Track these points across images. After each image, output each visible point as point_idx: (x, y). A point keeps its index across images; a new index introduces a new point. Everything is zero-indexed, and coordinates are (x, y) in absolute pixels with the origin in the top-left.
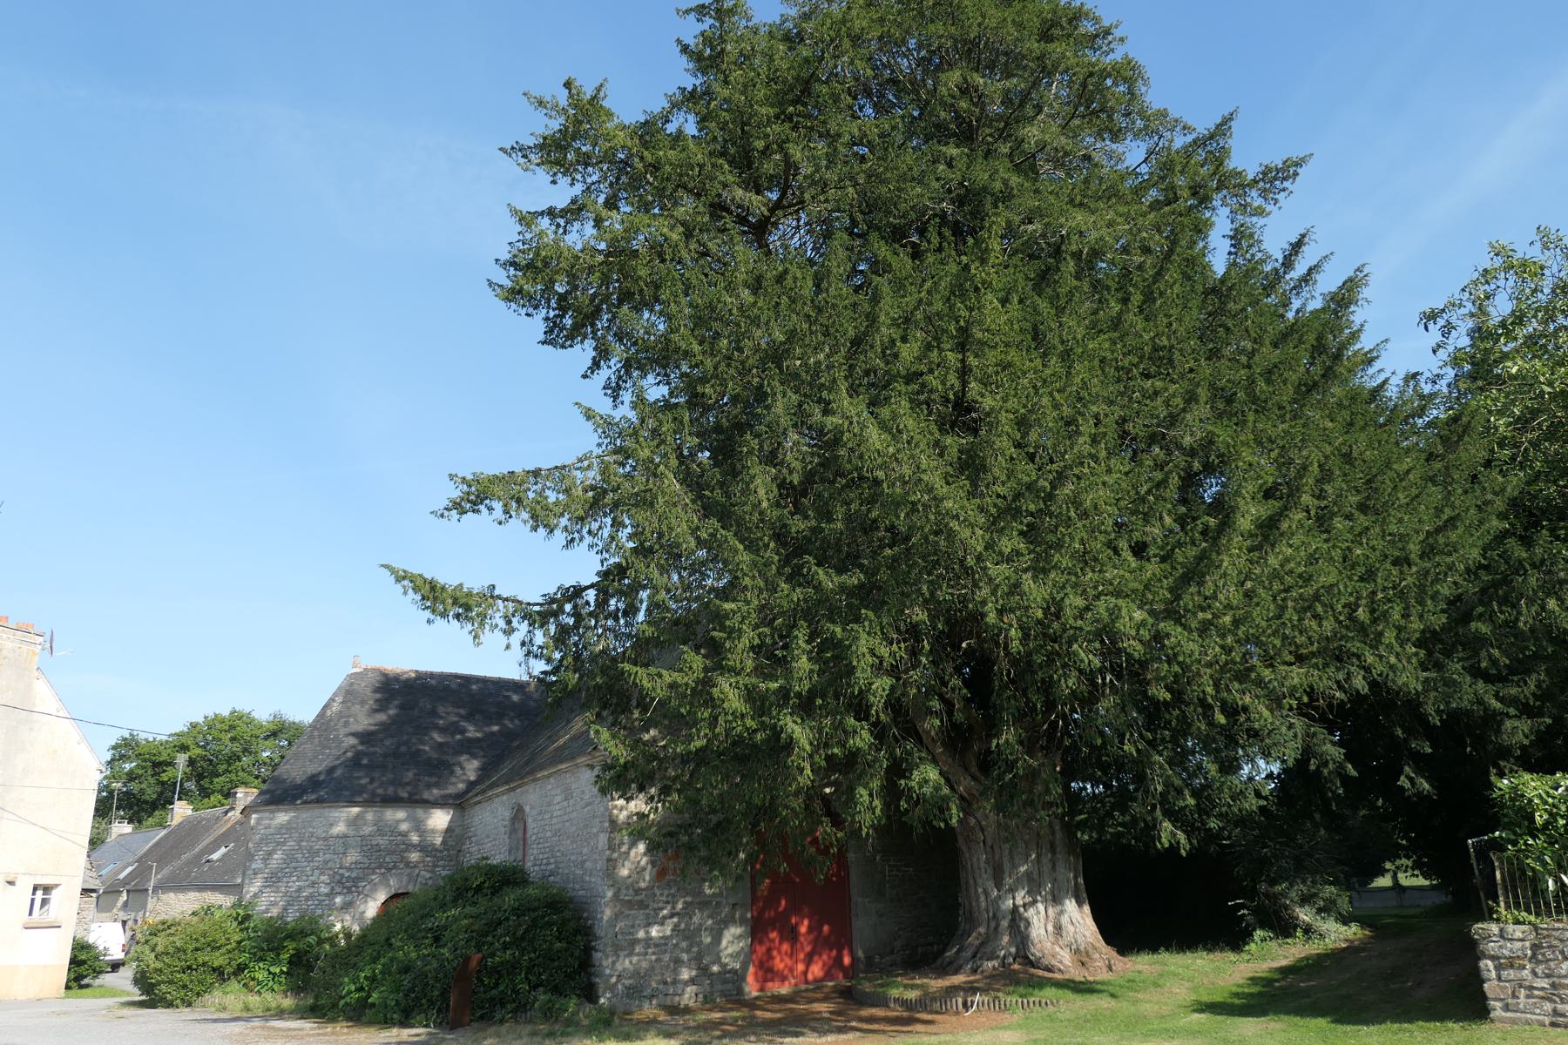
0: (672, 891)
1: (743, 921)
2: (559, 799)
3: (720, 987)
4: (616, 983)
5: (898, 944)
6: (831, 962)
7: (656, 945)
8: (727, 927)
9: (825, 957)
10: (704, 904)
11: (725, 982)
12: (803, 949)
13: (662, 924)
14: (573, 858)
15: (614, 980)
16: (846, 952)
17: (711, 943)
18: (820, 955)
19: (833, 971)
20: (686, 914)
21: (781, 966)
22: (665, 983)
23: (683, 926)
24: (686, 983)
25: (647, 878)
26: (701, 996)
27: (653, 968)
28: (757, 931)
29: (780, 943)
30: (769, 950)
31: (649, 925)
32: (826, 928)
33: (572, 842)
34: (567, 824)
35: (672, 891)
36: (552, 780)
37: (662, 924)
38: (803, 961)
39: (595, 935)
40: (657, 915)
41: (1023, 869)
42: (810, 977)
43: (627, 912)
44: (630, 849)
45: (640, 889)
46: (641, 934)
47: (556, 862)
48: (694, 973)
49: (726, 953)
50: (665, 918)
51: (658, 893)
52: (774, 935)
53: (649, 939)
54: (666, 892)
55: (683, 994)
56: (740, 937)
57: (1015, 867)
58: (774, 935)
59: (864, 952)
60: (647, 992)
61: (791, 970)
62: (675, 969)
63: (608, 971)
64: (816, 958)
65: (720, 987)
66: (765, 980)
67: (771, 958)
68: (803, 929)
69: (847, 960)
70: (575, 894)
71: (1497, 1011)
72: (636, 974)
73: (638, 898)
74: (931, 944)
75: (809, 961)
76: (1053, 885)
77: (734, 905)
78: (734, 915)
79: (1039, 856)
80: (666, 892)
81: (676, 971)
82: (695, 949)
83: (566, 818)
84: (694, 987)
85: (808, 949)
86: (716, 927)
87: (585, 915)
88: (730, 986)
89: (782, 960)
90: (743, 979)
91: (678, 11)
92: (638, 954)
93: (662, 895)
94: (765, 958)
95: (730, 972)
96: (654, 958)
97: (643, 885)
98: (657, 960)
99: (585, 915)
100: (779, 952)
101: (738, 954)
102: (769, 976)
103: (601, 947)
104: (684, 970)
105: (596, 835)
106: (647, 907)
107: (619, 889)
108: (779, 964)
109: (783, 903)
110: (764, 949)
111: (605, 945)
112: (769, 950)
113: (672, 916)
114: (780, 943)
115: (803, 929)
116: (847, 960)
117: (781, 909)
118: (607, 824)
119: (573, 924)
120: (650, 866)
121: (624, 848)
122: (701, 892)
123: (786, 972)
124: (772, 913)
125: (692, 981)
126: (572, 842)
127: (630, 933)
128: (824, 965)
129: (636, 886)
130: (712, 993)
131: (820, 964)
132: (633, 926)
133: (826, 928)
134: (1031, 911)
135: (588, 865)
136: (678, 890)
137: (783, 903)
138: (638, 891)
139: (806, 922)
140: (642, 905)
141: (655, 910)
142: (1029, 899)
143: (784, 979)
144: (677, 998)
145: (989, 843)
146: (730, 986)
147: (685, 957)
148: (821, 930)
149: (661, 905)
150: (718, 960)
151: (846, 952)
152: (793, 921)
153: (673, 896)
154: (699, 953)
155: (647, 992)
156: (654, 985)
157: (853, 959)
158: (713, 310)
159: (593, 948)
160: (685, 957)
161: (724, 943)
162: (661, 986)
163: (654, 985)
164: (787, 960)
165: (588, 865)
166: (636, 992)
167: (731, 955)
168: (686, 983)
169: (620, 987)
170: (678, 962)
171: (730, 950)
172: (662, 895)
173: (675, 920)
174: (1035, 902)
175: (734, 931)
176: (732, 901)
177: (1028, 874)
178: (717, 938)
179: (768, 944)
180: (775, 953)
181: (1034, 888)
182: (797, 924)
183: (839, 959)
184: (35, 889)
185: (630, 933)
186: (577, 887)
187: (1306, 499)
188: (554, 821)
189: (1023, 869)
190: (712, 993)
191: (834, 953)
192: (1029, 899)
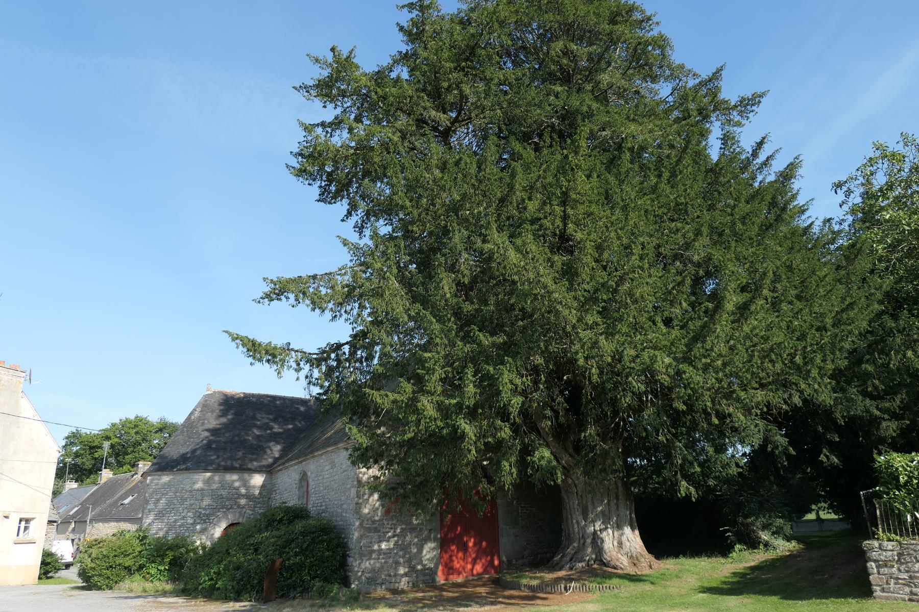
0: (394, 522)
1: (435, 540)
2: (327, 468)
3: (422, 578)
4: (361, 576)
5: (526, 553)
6: (487, 563)
7: (385, 554)
8: (426, 543)
9: (483, 560)
10: (413, 529)
11: (425, 575)
12: (470, 556)
13: (388, 541)
14: (336, 502)
15: (360, 574)
16: (496, 558)
17: (417, 552)
18: (481, 559)
19: (488, 569)
20: (402, 535)
21: (458, 566)
22: (390, 576)
23: (400, 542)
24: (402, 576)
25: (379, 514)
26: (411, 583)
27: (382, 567)
28: (444, 545)
29: (457, 552)
30: (451, 556)
31: (380, 542)
32: (484, 544)
33: (335, 493)
34: (332, 483)
35: (394, 522)
36: (323, 457)
37: (388, 541)
38: (471, 563)
39: (349, 548)
40: (385, 536)
41: (599, 509)
42: (475, 572)
43: (368, 534)
44: (369, 497)
45: (375, 521)
46: (376, 547)
47: (326, 505)
48: (407, 570)
49: (426, 558)
50: (390, 537)
51: (386, 523)
52: (453, 548)
53: (380, 550)
54: (390, 523)
55: (400, 582)
56: (433, 549)
57: (595, 508)
58: (453, 548)
59: (506, 558)
60: (379, 581)
61: (464, 568)
62: (396, 568)
63: (356, 569)
64: (478, 561)
65: (422, 578)
66: (449, 574)
67: (452, 561)
68: (471, 544)
69: (496, 562)
70: (337, 523)
71: (878, 592)
72: (373, 570)
73: (374, 526)
74: (546, 553)
75: (474, 563)
76: (617, 518)
77: (430, 530)
78: (430, 536)
79: (609, 501)
80: (390, 523)
81: (396, 569)
82: (407, 556)
83: (332, 479)
84: (407, 578)
85: (474, 556)
86: (420, 543)
87: (343, 536)
88: (428, 578)
89: (458, 562)
90: (436, 573)
91: (397, 6)
92: (374, 559)
93: (388, 524)
94: (448, 561)
95: (428, 569)
96: (383, 561)
97: (377, 518)
98: (385, 562)
99: (343, 536)
100: (457, 557)
101: (433, 558)
102: (451, 571)
103: (352, 555)
104: (401, 568)
105: (349, 489)
106: (379, 531)
107: (363, 521)
108: (457, 565)
109: (459, 529)
110: (448, 556)
111: (355, 553)
112: (451, 556)
113: (394, 536)
114: (457, 552)
115: (471, 544)
116: (496, 562)
117: (457, 532)
118: (356, 483)
119: (336, 541)
120: (381, 507)
121: (366, 497)
122: (411, 523)
123: (460, 569)
124: (453, 535)
125: (406, 575)
126: (335, 493)
127: (369, 547)
128: (483, 565)
129: (373, 519)
130: (417, 582)
131: (481, 564)
132: (371, 543)
133: (484, 544)
134: (604, 534)
135: (345, 506)
136: (398, 521)
137: (459, 529)
138: (374, 522)
139: (472, 540)
140: (376, 530)
141: (384, 533)
142: (603, 527)
143: (459, 573)
144: (397, 585)
145: (580, 494)
146: (428, 578)
147: (401, 560)
148: (481, 545)
149: (387, 530)
150: (421, 562)
151: (496, 558)
152: (465, 539)
153: (395, 525)
154: (410, 558)
155: (379, 581)
156: (383, 577)
157: (500, 562)
158: (418, 181)
159: (348, 555)
160: (401, 560)
161: (424, 552)
162: (387, 578)
163: (383, 577)
164: (461, 562)
165: (345, 506)
166: (373, 581)
167: (428, 559)
168: (402, 576)
169: (363, 578)
170: (397, 563)
171: (428, 557)
172: (388, 524)
173: (396, 539)
174: (606, 528)
175: (430, 545)
176: (429, 527)
177: (602, 512)
178: (420, 550)
179: (450, 553)
180: (454, 558)
181: (606, 520)
182: (467, 541)
183: (492, 562)
184: (21, 520)
185: (369, 547)
186: (338, 519)
187: (765, 292)
188: (325, 481)
189: (599, 509)
190: (417, 582)
191: (489, 558)
192: (603, 527)
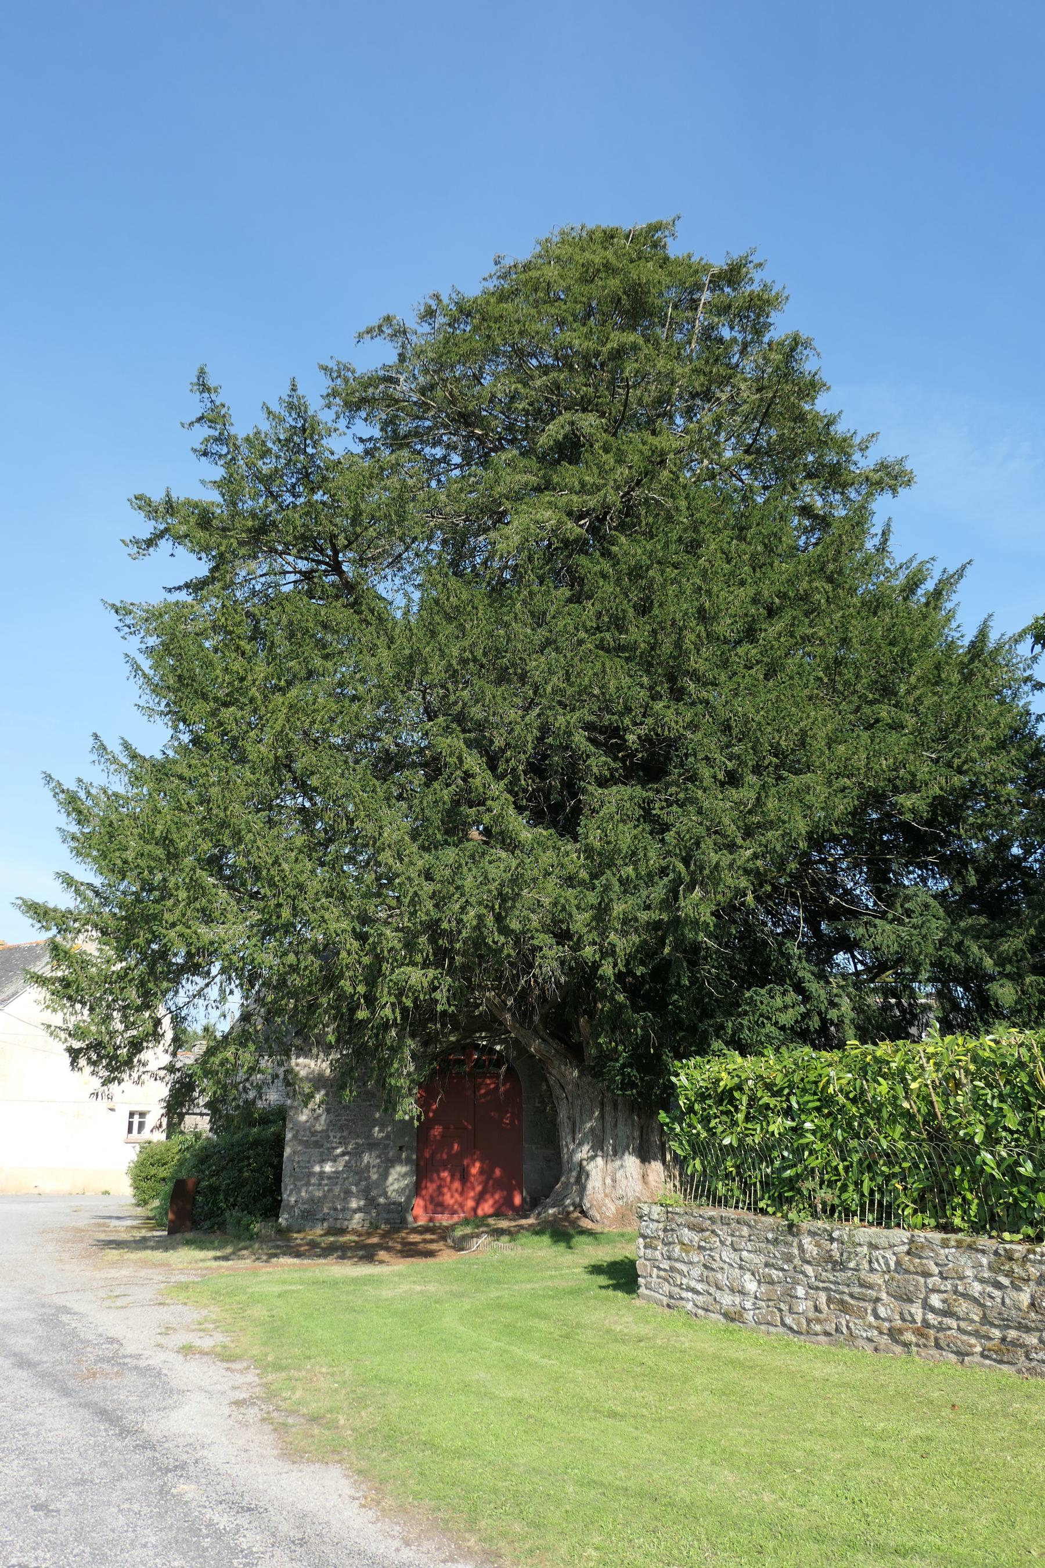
0: (345, 1134)
1: (408, 1161)
3: (385, 1216)
6: (501, 1201)
7: (329, 1178)
8: (393, 1166)
9: (497, 1196)
10: (372, 1145)
12: (473, 1189)
13: (335, 1161)
17: (378, 1179)
18: (492, 1195)
20: (357, 1153)
21: (451, 1202)
22: (336, 1209)
24: (355, 1211)
25: (322, 1122)
27: (325, 1197)
28: (423, 1172)
29: (452, 1181)
30: (440, 1187)
32: (498, 1172)
35: (345, 1134)
37: (335, 1161)
38: (473, 1198)
40: (330, 1153)
41: (588, 1125)
42: (480, 1212)
45: (316, 1132)
46: (317, 1169)
48: (362, 1203)
49: (391, 1188)
50: (338, 1156)
51: (331, 1134)
52: (445, 1174)
53: (322, 1173)
54: (339, 1135)
55: (351, 1219)
56: (404, 1176)
57: (583, 1123)
58: (445, 1174)
60: (319, 1216)
61: (462, 1206)
64: (488, 1196)
65: (385, 1216)
68: (474, 1170)
71: (642, 1290)
72: (312, 1200)
73: (313, 1139)
75: (479, 1199)
76: (615, 1141)
79: (602, 1116)
80: (339, 1135)
81: (345, 1200)
82: (364, 1183)
84: (362, 1215)
85: (479, 1188)
88: (395, 1216)
89: (452, 1196)
91: (183, 425)
92: (314, 1185)
93: (335, 1137)
94: (435, 1194)
95: (394, 1203)
96: (326, 1188)
97: (318, 1128)
98: (329, 1190)
101: (403, 1189)
102: (439, 1209)
104: (353, 1199)
106: (322, 1146)
107: (298, 1131)
108: (449, 1199)
109: (456, 1146)
110: (434, 1186)
112: (440, 1187)
113: (343, 1154)
114: (452, 1181)
115: (474, 1170)
122: (370, 1135)
124: (445, 1156)
125: (359, 1210)
127: (306, 1167)
128: (495, 1203)
129: (313, 1130)
131: (491, 1202)
132: (309, 1162)
133: (498, 1172)
134: (592, 1164)
136: (350, 1133)
138: (314, 1133)
139: (478, 1165)
140: (317, 1145)
141: (328, 1149)
142: (591, 1153)
143: (454, 1212)
144: (346, 1223)
145: (570, 1099)
146: (395, 1216)
147: (354, 1189)
148: (493, 1171)
149: (334, 1145)
150: (385, 1194)
153: (345, 1138)
154: (367, 1187)
155: (319, 1216)
156: (326, 1210)
160: (354, 1189)
161: (390, 1179)
163: (326, 1210)
164: (457, 1195)
166: (309, 1215)
167: (397, 1191)
168: (355, 1211)
170: (348, 1193)
171: (396, 1186)
173: (347, 1158)
174: (596, 1156)
175: (400, 1169)
177: (592, 1129)
178: (385, 1176)
179: (438, 1183)
180: (445, 1190)
181: (598, 1146)
182: (468, 1166)
184: (132, 1115)
185: (306, 1167)
187: (556, 783)
189: (588, 1125)
192: (591, 1153)
